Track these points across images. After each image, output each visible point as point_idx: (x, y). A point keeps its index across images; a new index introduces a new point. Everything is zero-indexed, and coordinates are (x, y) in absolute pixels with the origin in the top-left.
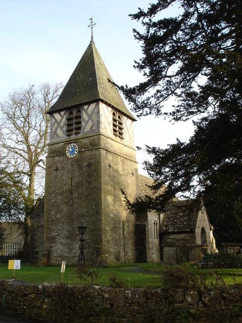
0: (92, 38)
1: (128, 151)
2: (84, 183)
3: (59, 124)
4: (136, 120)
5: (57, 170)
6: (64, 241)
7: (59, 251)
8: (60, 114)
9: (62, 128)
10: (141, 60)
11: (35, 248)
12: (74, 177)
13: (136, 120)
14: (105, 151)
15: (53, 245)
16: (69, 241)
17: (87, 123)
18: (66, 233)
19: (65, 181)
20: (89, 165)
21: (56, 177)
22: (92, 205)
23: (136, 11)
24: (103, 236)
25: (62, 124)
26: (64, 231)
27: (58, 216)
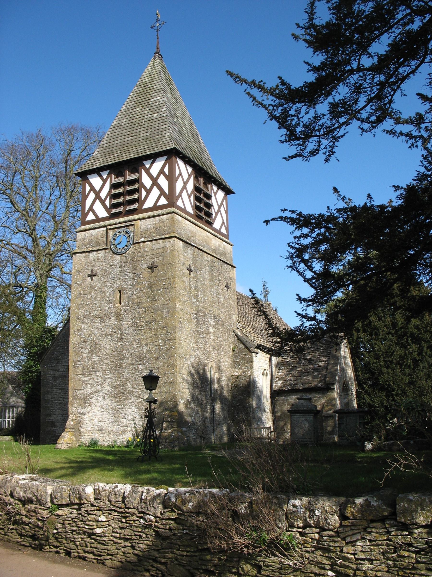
0: (237, 78)
1: (219, 246)
2: (144, 299)
3: (97, 194)
4: (233, 193)
5: (92, 275)
6: (107, 403)
7: (96, 421)
8: (100, 176)
9: (103, 202)
10: (407, 142)
11: (50, 416)
12: (125, 289)
13: (233, 193)
14: (181, 243)
15: (85, 410)
16: (115, 404)
17: (148, 192)
18: (110, 389)
19: (108, 295)
20: (152, 268)
21: (92, 288)
22: (157, 338)
23: (306, 61)
24: (145, 425)
25: (103, 195)
26: (106, 385)
27: (95, 358)
